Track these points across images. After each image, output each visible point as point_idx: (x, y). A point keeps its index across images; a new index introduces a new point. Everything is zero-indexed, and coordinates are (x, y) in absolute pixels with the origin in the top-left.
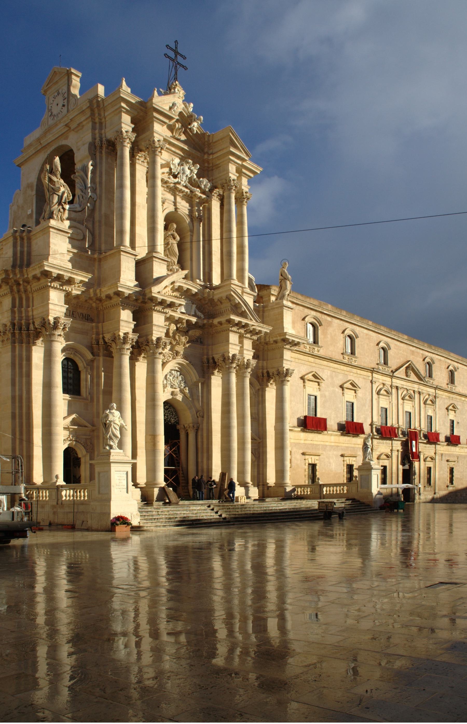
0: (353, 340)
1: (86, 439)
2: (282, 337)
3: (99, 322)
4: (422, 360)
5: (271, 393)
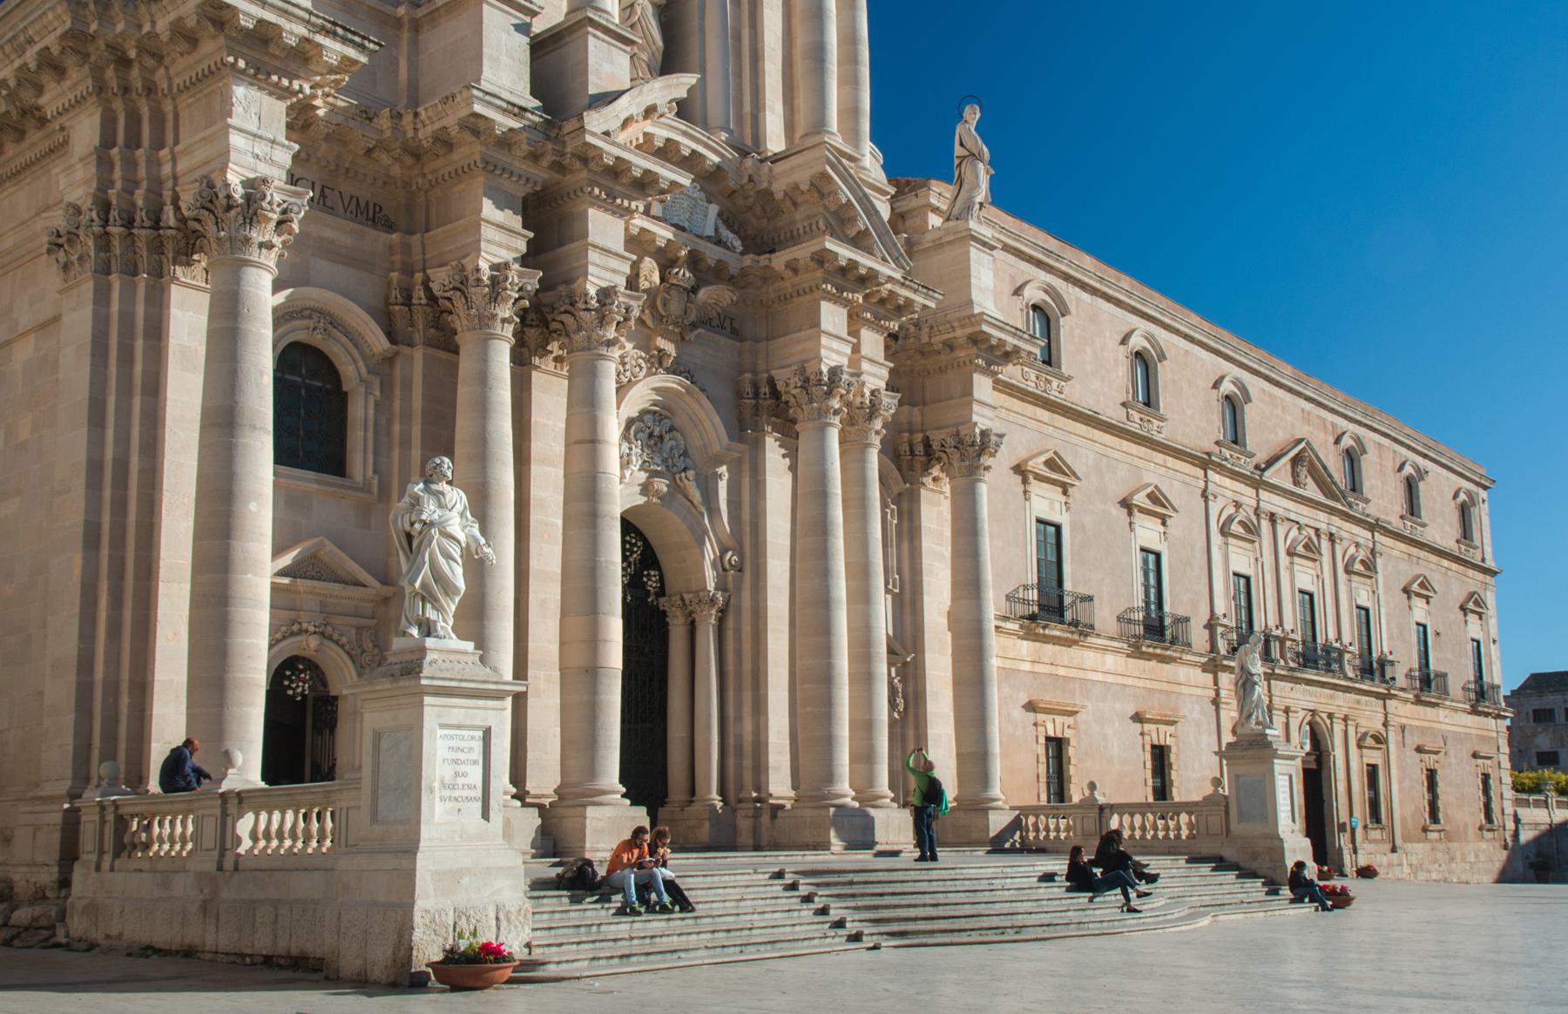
0: (1151, 366)
1: (358, 628)
2: (969, 330)
3: (411, 232)
4: (1331, 440)
5: (936, 508)
